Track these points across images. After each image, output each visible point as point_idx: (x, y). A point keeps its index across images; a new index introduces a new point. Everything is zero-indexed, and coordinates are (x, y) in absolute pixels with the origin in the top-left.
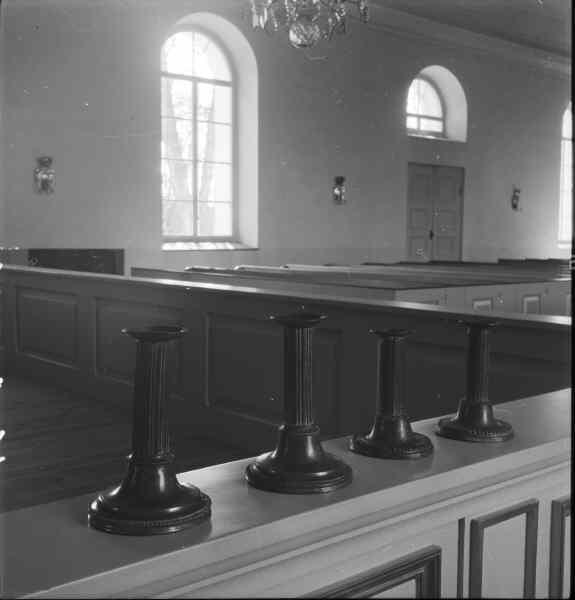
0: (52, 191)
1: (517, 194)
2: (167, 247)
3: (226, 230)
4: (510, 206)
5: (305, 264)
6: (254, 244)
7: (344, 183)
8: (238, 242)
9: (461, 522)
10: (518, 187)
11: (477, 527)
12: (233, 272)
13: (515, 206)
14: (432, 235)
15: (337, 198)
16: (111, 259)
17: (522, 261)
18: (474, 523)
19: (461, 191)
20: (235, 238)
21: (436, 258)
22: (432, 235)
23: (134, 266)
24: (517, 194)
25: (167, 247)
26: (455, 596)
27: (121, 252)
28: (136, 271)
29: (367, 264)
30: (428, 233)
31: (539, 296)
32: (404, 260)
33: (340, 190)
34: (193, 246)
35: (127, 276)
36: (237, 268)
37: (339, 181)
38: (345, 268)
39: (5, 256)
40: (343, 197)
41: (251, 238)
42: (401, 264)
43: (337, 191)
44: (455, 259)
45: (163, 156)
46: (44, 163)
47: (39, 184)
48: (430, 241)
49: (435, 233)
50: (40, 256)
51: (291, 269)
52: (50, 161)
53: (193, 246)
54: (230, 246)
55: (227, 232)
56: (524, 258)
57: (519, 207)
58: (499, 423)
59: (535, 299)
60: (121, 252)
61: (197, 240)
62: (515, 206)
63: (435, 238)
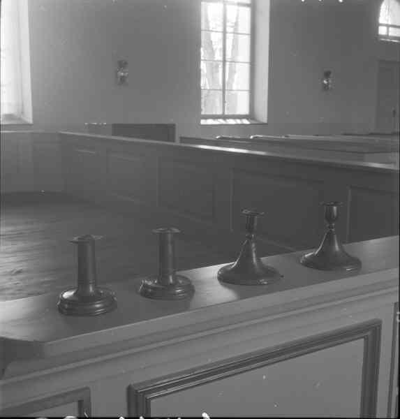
3: (243, 109)
7: (331, 75)
15: (325, 87)
20: (251, 116)
25: (203, 122)
28: (183, 139)
29: (346, 134)
33: (327, 81)
34: (221, 121)
35: (177, 143)
37: (327, 75)
40: (330, 86)
41: (263, 115)
42: (372, 134)
43: (325, 82)
47: (119, 79)
50: (119, 129)
53: (221, 121)
54: (246, 122)
60: (174, 125)
61: (225, 117)
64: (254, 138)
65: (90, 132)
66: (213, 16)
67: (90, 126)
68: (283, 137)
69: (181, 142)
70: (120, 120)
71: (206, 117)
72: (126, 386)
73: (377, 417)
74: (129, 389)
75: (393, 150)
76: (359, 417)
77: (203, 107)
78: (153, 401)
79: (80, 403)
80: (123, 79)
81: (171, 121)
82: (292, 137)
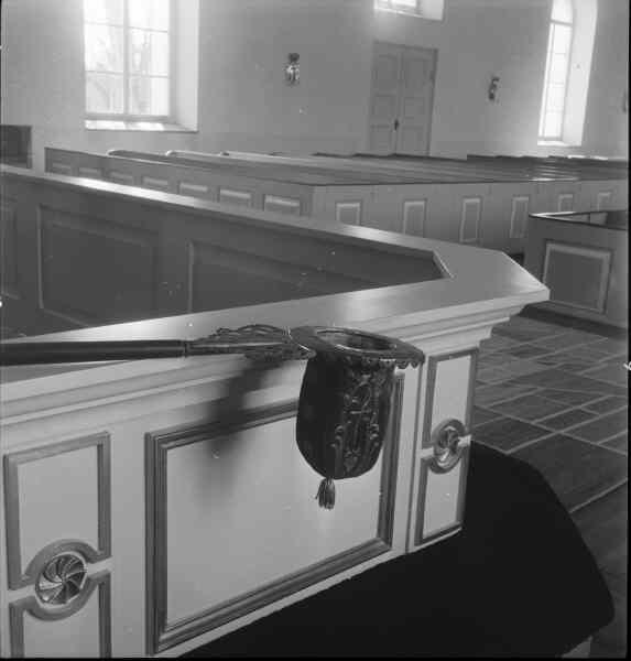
1: (495, 82)
2: (89, 124)
3: (160, 106)
4: (487, 95)
8: (175, 123)
10: (497, 75)
12: (163, 158)
13: (492, 97)
14: (397, 124)
15: (291, 79)
17: (492, 158)
19: (433, 78)
22: (397, 124)
24: (495, 82)
25: (89, 124)
27: (28, 129)
28: (54, 157)
29: (318, 154)
30: (393, 122)
31: (529, 196)
33: (294, 69)
34: (121, 125)
35: (38, 168)
36: (168, 153)
37: (294, 58)
41: (190, 120)
43: (290, 70)
44: (423, 153)
53: (121, 125)
54: (159, 127)
55: (555, 134)
56: (520, 155)
57: (496, 98)
58: (349, 358)
59: (607, 194)
60: (28, 129)
61: (129, 119)
62: (492, 97)
63: (400, 128)
64: (172, 154)
66: (560, 11)
68: (219, 155)
69: (49, 168)
71: (94, 117)
72: (143, 436)
74: (147, 436)
78: (169, 452)
79: (100, 447)
82: (235, 155)
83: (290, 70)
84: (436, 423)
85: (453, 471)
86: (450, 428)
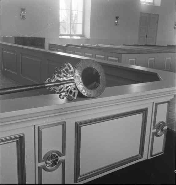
0: (25, 19)
3: (80, 32)
5: (103, 44)
6: (89, 38)
7: (119, 19)
9: (153, 103)
11: (157, 104)
14: (146, 36)
15: (116, 24)
16: (39, 42)
18: (156, 103)
19: (157, 22)
20: (82, 36)
21: (147, 44)
22: (146, 36)
23: (49, 43)
25: (60, 37)
26: (61, 183)
27: (44, 38)
29: (124, 45)
30: (145, 36)
32: (137, 44)
35: (47, 49)
37: (117, 18)
38: (116, 46)
39: (5, 39)
40: (118, 23)
41: (88, 36)
42: (135, 45)
43: (116, 21)
44: (154, 44)
45: (60, 8)
46: (23, 10)
47: (21, 16)
48: (146, 38)
49: (147, 35)
50: (21, 40)
51: (99, 46)
52: (25, 9)
53: (69, 37)
54: (79, 38)
60: (44, 38)
61: (71, 35)
65: (4, 41)
67: (4, 37)
68: (96, 45)
69: (50, 49)
70: (21, 35)
73: (27, 183)
75: (175, 53)
76: (17, 183)
77: (60, 32)
80: (23, 17)
81: (43, 37)
82: (100, 45)
83: (116, 21)
84: (157, 122)
85: (162, 136)
86: (161, 124)
